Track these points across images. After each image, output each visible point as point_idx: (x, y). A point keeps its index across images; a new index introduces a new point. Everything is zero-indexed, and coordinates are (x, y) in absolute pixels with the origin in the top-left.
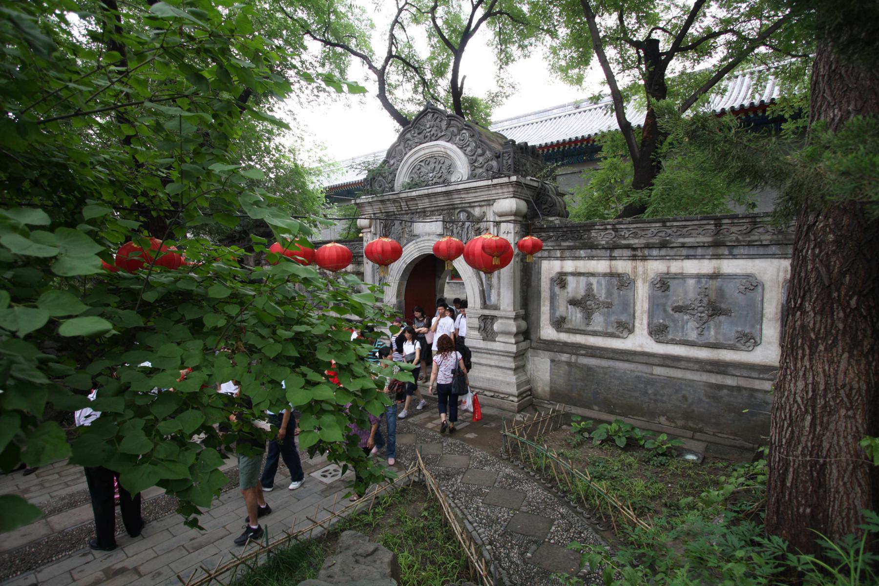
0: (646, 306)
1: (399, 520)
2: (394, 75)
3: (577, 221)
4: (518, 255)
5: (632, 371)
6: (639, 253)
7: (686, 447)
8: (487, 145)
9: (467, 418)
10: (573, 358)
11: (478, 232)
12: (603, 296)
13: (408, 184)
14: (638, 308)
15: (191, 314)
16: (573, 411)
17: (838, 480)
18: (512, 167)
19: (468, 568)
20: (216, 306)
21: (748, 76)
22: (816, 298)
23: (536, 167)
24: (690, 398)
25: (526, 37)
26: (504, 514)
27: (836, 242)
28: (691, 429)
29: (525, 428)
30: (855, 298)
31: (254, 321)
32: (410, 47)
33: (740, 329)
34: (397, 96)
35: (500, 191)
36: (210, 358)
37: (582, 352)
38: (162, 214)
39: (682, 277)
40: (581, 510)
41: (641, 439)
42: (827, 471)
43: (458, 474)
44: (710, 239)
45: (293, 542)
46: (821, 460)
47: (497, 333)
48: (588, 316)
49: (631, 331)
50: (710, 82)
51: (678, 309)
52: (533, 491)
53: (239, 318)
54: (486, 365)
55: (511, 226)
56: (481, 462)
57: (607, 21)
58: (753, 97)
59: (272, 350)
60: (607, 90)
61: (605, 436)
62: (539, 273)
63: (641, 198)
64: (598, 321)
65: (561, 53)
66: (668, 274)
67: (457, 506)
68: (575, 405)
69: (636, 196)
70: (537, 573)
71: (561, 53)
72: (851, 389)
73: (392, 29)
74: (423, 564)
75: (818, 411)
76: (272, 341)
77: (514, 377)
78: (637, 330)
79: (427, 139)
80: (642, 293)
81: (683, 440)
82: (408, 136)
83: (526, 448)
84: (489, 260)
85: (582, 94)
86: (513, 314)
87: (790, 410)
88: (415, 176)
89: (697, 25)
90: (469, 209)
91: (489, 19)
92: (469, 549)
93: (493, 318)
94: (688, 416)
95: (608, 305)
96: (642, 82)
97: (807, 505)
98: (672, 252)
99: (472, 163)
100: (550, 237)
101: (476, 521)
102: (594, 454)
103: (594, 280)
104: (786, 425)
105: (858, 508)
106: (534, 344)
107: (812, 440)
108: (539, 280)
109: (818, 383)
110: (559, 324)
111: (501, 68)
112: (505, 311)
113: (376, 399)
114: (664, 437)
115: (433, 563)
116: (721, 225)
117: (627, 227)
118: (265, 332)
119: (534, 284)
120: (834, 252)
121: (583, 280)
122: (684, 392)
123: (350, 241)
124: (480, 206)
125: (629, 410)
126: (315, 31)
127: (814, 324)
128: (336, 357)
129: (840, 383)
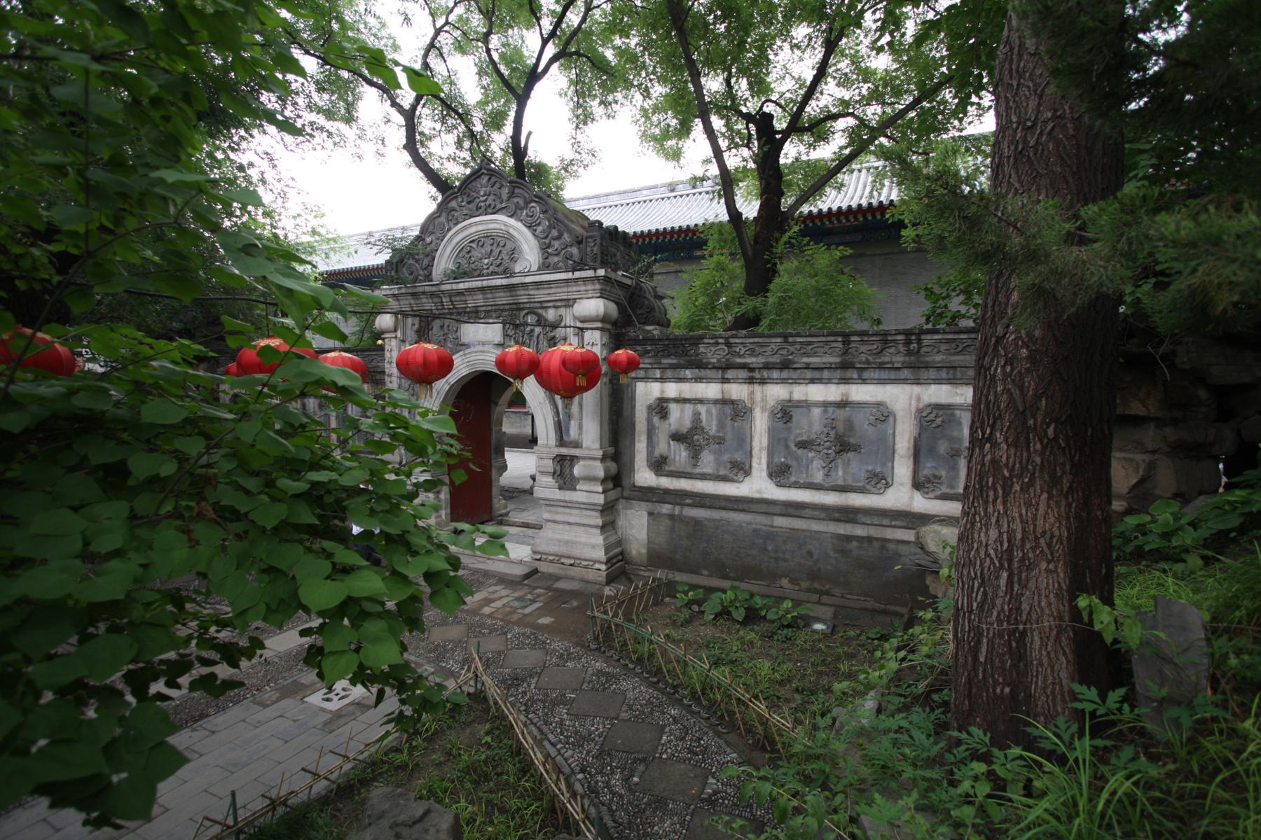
0: (765, 442)
1: (449, 754)
2: (428, 121)
3: (677, 332)
4: (606, 374)
5: (749, 523)
6: (757, 375)
7: (812, 614)
8: (566, 226)
9: (539, 596)
10: (677, 510)
11: (553, 342)
12: (714, 428)
13: (453, 271)
14: (756, 444)
15: (101, 453)
16: (677, 579)
17: (1040, 649)
18: (599, 257)
19: (553, 810)
20: (152, 438)
21: (864, 171)
22: (1009, 427)
23: (627, 260)
24: (816, 553)
25: (613, 90)
26: (598, 727)
27: (1031, 358)
28: (816, 591)
29: (619, 606)
30: (1053, 426)
31: (229, 466)
32: (452, 83)
33: (870, 468)
34: (432, 150)
35: (583, 288)
36: (143, 533)
37: (688, 501)
38: (38, 287)
39: (806, 405)
40: (697, 709)
41: (761, 609)
42: (1028, 639)
43: (531, 676)
44: (838, 360)
45: (281, 810)
46: (1021, 627)
47: (578, 480)
48: (695, 455)
49: (748, 473)
50: (825, 176)
51: (803, 445)
52: (635, 689)
53: (204, 460)
54: (563, 523)
55: (597, 334)
56: (562, 655)
57: (713, 84)
58: (871, 196)
59: (269, 515)
60: (714, 170)
61: (719, 609)
62: (633, 398)
63: (755, 308)
64: (708, 461)
65: (655, 118)
66: (790, 401)
67: (532, 723)
68: (679, 570)
69: (750, 304)
70: (647, 804)
71: (655, 118)
72: (1052, 537)
73: (426, 56)
74: (489, 814)
75: (1016, 565)
76: (265, 498)
77: (601, 538)
78: (754, 471)
79: (480, 211)
80: (760, 424)
81: (809, 605)
82: (453, 204)
83: (623, 631)
84: (569, 381)
85: (680, 174)
86: (599, 454)
87: (981, 565)
88: (464, 262)
89: (813, 103)
90: (540, 311)
91: (562, 61)
92: (556, 785)
93: (573, 459)
94: (814, 576)
95: (720, 441)
96: (752, 165)
97: (1005, 684)
98: (794, 375)
99: (544, 248)
100: (647, 352)
101: (560, 741)
102: (707, 632)
103: (702, 409)
104: (976, 585)
105: (1064, 682)
106: (626, 493)
107: (1010, 602)
108: (633, 407)
109: (1014, 531)
110: (659, 465)
111: (577, 127)
112: (589, 449)
113: (447, 586)
114: (788, 604)
115: (503, 810)
116: (849, 342)
117: (742, 341)
118: (251, 484)
119: (626, 413)
120: (1027, 370)
121: (689, 408)
122: (809, 547)
123: (363, 350)
124: (555, 307)
125: (746, 573)
126: (305, 40)
127: (1008, 459)
128: (383, 522)
129: (1039, 530)
